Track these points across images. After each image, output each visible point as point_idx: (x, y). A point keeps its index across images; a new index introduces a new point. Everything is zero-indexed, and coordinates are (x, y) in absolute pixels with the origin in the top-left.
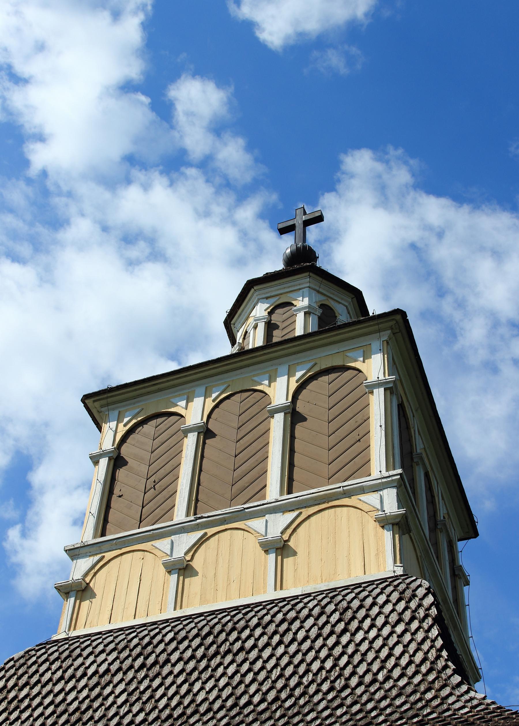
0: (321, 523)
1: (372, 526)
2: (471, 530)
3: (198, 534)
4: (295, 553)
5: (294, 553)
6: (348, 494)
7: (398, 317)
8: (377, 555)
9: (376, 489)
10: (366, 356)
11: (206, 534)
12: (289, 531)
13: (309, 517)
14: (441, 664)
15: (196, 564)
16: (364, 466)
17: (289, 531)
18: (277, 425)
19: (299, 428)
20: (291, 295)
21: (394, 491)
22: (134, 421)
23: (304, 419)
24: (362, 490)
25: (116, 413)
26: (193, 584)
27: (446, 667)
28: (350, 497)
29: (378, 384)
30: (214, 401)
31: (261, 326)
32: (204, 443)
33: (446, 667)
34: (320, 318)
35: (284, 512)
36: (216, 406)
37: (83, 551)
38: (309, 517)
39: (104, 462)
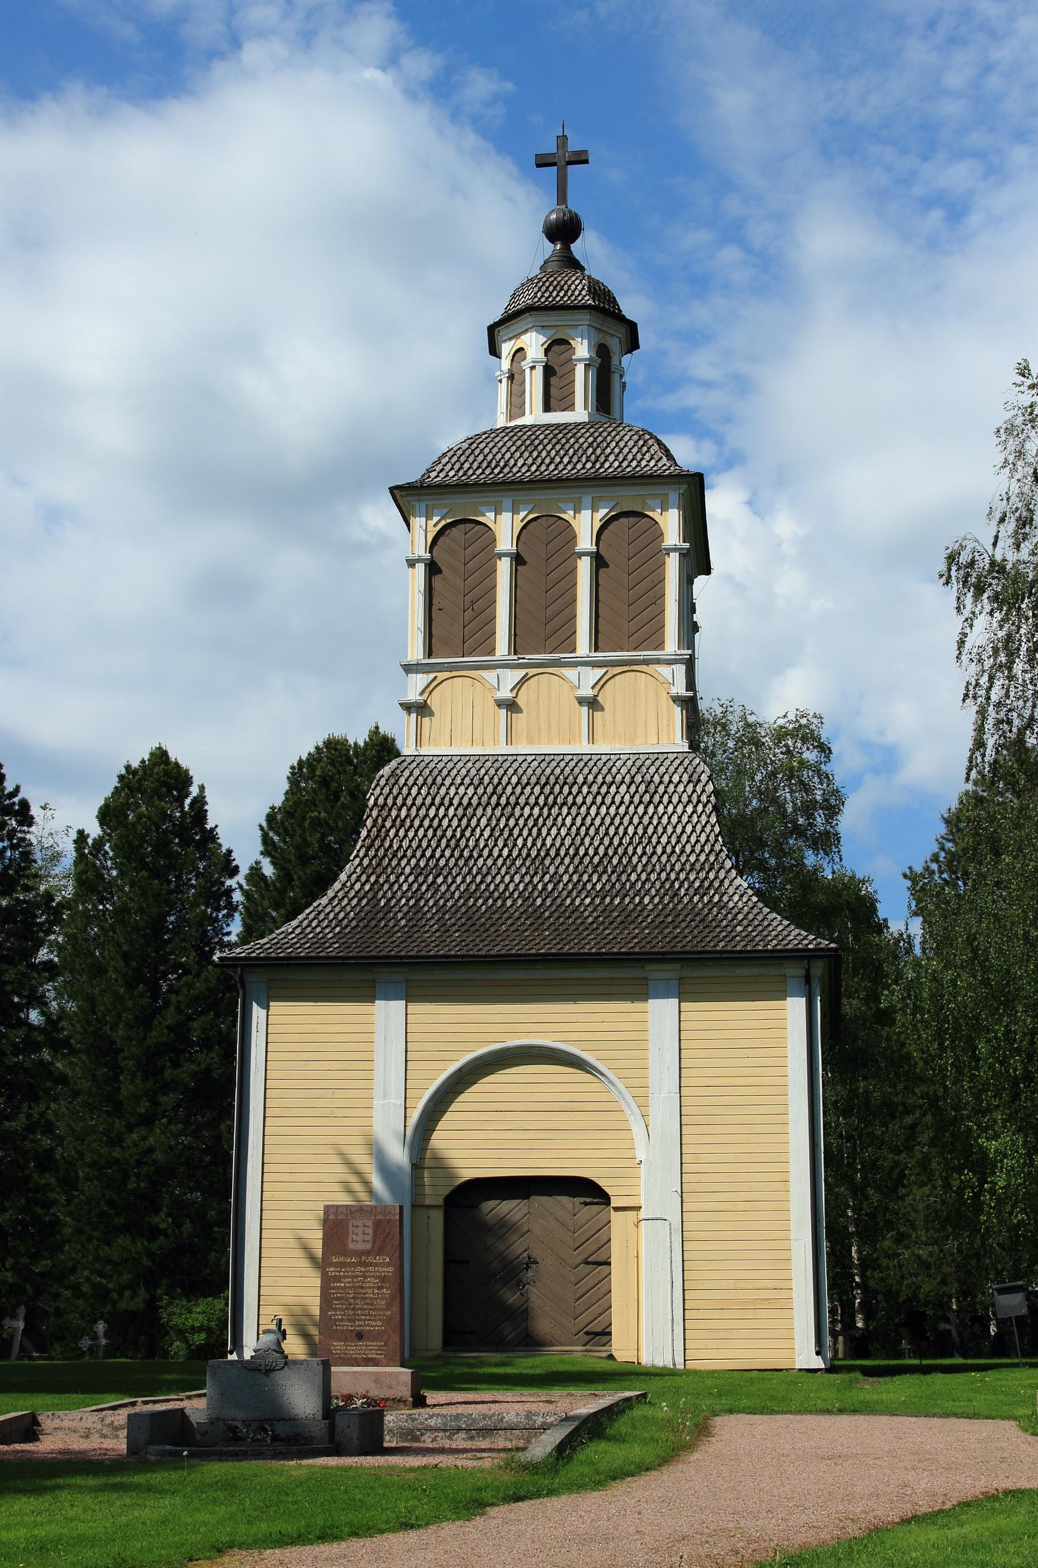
0: (624, 683)
1: (666, 702)
2: (707, 570)
3: (521, 673)
4: (602, 709)
5: (602, 709)
6: (647, 662)
7: (697, 478)
8: (668, 725)
9: (669, 662)
10: (664, 508)
11: (527, 674)
12: (598, 687)
13: (614, 676)
14: (717, 847)
15: (521, 701)
16: (660, 645)
17: (598, 687)
18: (584, 568)
19: (602, 571)
20: (570, 331)
21: (684, 667)
22: (443, 523)
23: (607, 566)
24: (658, 661)
25: (423, 506)
26: (520, 720)
27: (721, 851)
28: (647, 665)
29: (675, 550)
30: (522, 521)
31: (539, 371)
32: (516, 570)
33: (721, 851)
34: (598, 371)
35: (593, 667)
36: (524, 528)
37: (419, 667)
38: (614, 676)
39: (420, 568)
